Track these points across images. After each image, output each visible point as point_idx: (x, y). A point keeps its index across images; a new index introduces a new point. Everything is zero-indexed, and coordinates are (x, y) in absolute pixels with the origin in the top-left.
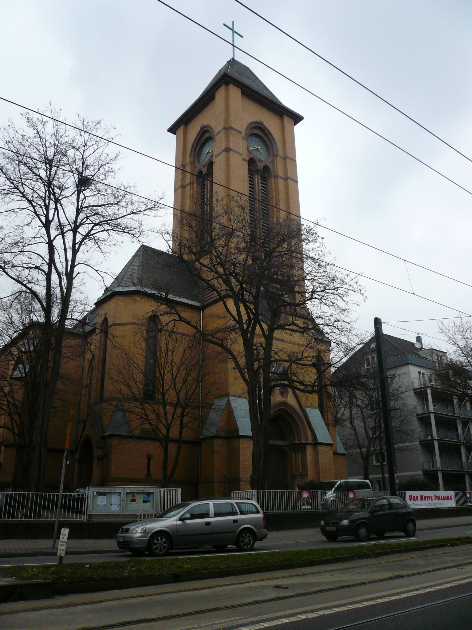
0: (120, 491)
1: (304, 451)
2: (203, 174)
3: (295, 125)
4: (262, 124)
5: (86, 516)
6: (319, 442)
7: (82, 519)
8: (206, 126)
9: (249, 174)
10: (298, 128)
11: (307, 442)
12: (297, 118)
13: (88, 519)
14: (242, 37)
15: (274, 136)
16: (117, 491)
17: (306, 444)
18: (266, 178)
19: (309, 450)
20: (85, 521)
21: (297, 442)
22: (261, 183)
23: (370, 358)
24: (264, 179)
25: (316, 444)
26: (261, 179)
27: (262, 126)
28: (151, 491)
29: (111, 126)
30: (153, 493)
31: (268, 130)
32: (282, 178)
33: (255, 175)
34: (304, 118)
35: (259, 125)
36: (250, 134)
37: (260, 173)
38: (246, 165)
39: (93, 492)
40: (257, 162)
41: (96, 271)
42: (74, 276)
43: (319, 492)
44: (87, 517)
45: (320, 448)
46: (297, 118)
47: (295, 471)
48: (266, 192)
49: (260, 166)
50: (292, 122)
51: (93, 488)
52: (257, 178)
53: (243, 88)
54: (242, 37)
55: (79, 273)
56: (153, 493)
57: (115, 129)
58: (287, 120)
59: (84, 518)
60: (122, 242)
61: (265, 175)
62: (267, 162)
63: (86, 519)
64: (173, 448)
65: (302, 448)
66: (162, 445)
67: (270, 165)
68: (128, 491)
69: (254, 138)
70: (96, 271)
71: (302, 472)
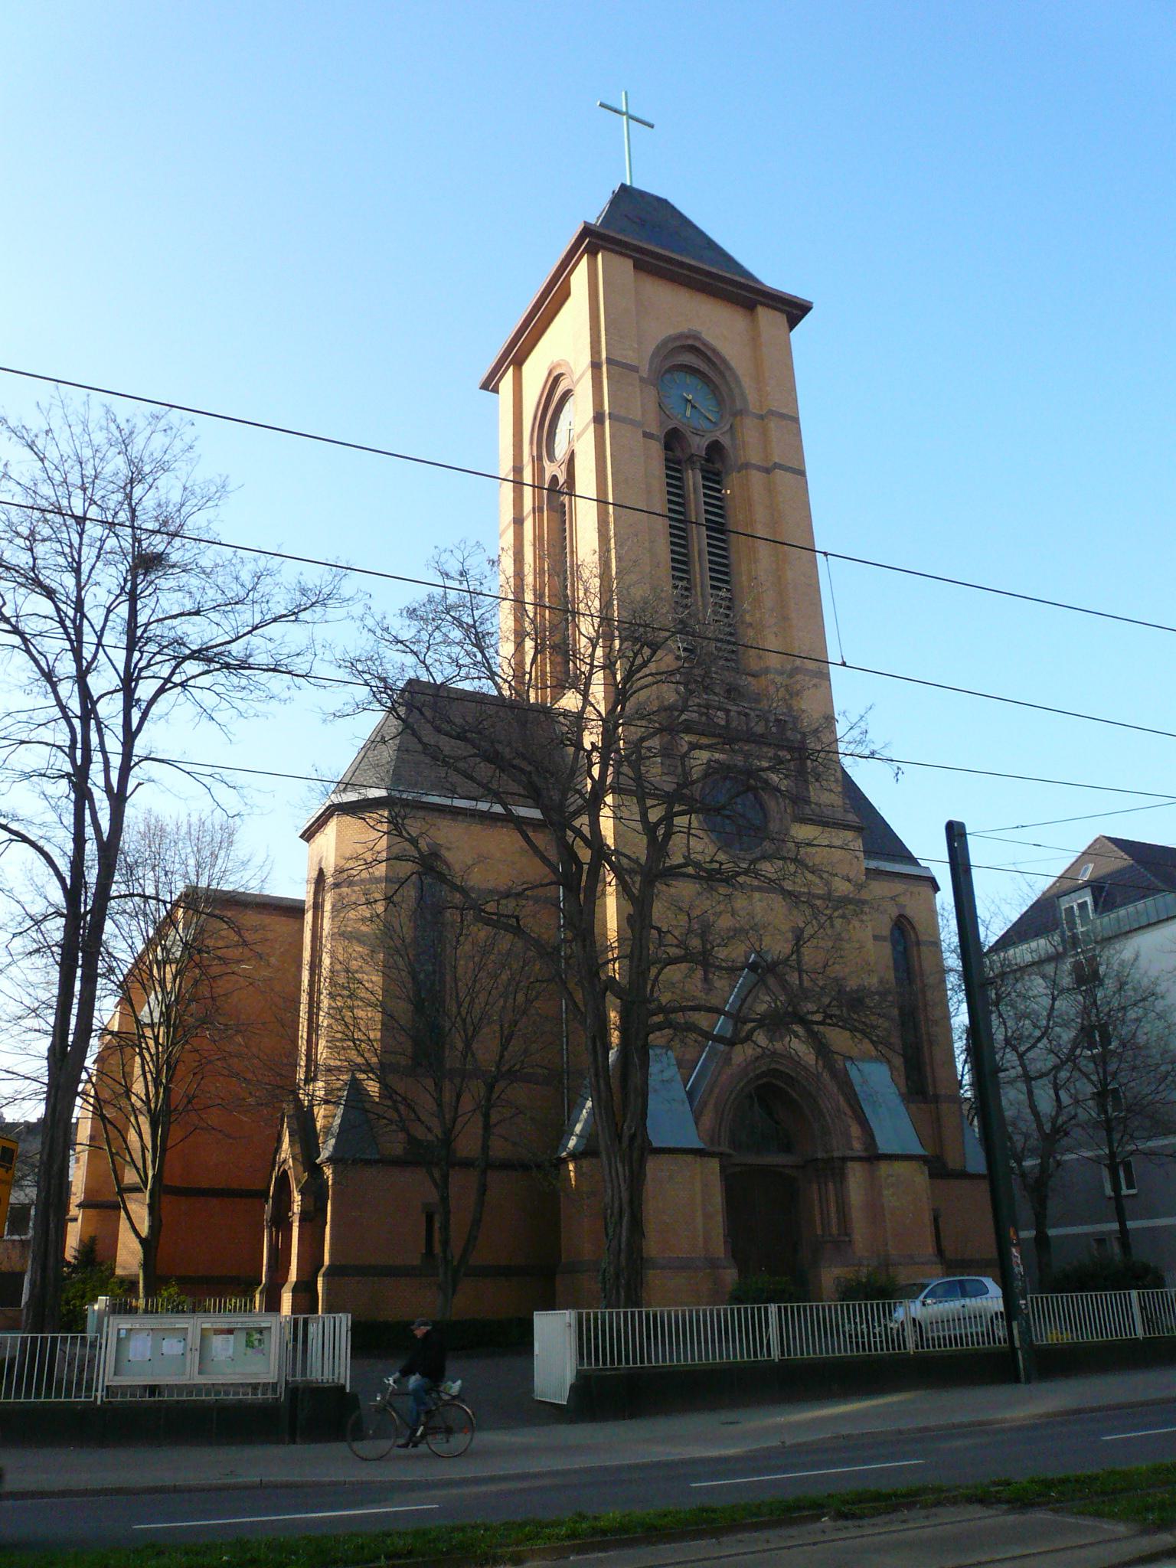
0: (186, 1326)
1: (841, 1177)
2: (560, 483)
3: (791, 328)
4: (696, 337)
5: (103, 1391)
6: (880, 1152)
7: (92, 1399)
8: (558, 365)
9: (668, 468)
10: (800, 335)
11: (849, 1153)
12: (795, 310)
13: (107, 1397)
14: (652, 126)
15: (733, 364)
16: (177, 1326)
17: (844, 1159)
18: (718, 474)
19: (856, 1177)
20: (99, 1402)
21: (820, 1155)
22: (705, 487)
23: (1075, 907)
24: (714, 477)
25: (873, 1157)
26: (704, 478)
27: (697, 344)
28: (264, 1325)
29: (182, 419)
30: (270, 1328)
31: (714, 350)
32: (759, 468)
33: (687, 470)
34: (814, 305)
35: (690, 342)
36: (663, 370)
37: (698, 465)
38: (656, 448)
39: (119, 1330)
40: (688, 434)
41: (188, 773)
42: (128, 794)
43: (773, 1308)
44: (105, 1393)
45: (884, 1168)
46: (795, 310)
47: (819, 1232)
48: (720, 508)
49: (698, 445)
50: (782, 319)
51: (118, 1321)
52: (693, 479)
53: (637, 255)
54: (652, 126)
55: (140, 784)
56: (270, 1328)
57: (193, 424)
58: (766, 317)
59: (96, 1397)
60: (289, 688)
61: (716, 466)
62: (718, 433)
63: (102, 1397)
64: (461, 1184)
65: (834, 1169)
66: (432, 1176)
67: (725, 441)
68: (205, 1326)
69: (680, 377)
70: (188, 773)
71: (839, 1235)
